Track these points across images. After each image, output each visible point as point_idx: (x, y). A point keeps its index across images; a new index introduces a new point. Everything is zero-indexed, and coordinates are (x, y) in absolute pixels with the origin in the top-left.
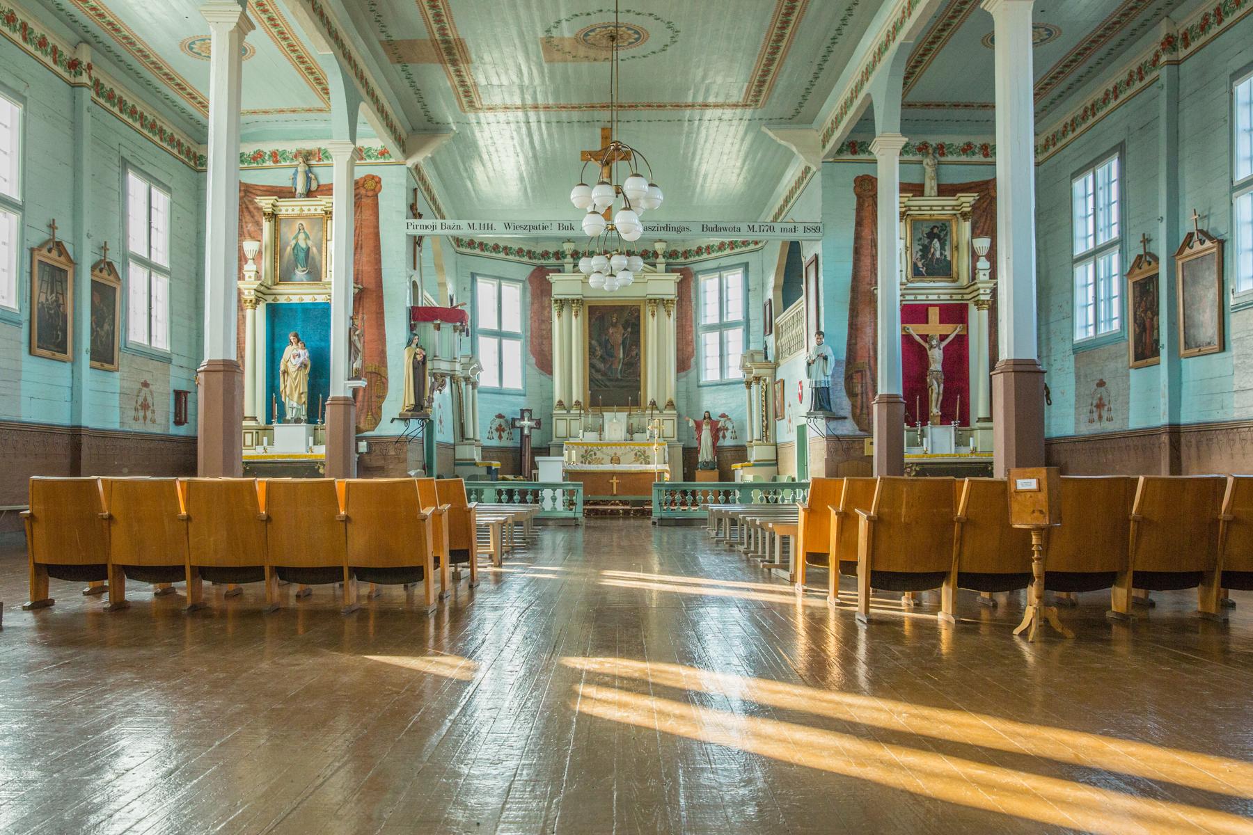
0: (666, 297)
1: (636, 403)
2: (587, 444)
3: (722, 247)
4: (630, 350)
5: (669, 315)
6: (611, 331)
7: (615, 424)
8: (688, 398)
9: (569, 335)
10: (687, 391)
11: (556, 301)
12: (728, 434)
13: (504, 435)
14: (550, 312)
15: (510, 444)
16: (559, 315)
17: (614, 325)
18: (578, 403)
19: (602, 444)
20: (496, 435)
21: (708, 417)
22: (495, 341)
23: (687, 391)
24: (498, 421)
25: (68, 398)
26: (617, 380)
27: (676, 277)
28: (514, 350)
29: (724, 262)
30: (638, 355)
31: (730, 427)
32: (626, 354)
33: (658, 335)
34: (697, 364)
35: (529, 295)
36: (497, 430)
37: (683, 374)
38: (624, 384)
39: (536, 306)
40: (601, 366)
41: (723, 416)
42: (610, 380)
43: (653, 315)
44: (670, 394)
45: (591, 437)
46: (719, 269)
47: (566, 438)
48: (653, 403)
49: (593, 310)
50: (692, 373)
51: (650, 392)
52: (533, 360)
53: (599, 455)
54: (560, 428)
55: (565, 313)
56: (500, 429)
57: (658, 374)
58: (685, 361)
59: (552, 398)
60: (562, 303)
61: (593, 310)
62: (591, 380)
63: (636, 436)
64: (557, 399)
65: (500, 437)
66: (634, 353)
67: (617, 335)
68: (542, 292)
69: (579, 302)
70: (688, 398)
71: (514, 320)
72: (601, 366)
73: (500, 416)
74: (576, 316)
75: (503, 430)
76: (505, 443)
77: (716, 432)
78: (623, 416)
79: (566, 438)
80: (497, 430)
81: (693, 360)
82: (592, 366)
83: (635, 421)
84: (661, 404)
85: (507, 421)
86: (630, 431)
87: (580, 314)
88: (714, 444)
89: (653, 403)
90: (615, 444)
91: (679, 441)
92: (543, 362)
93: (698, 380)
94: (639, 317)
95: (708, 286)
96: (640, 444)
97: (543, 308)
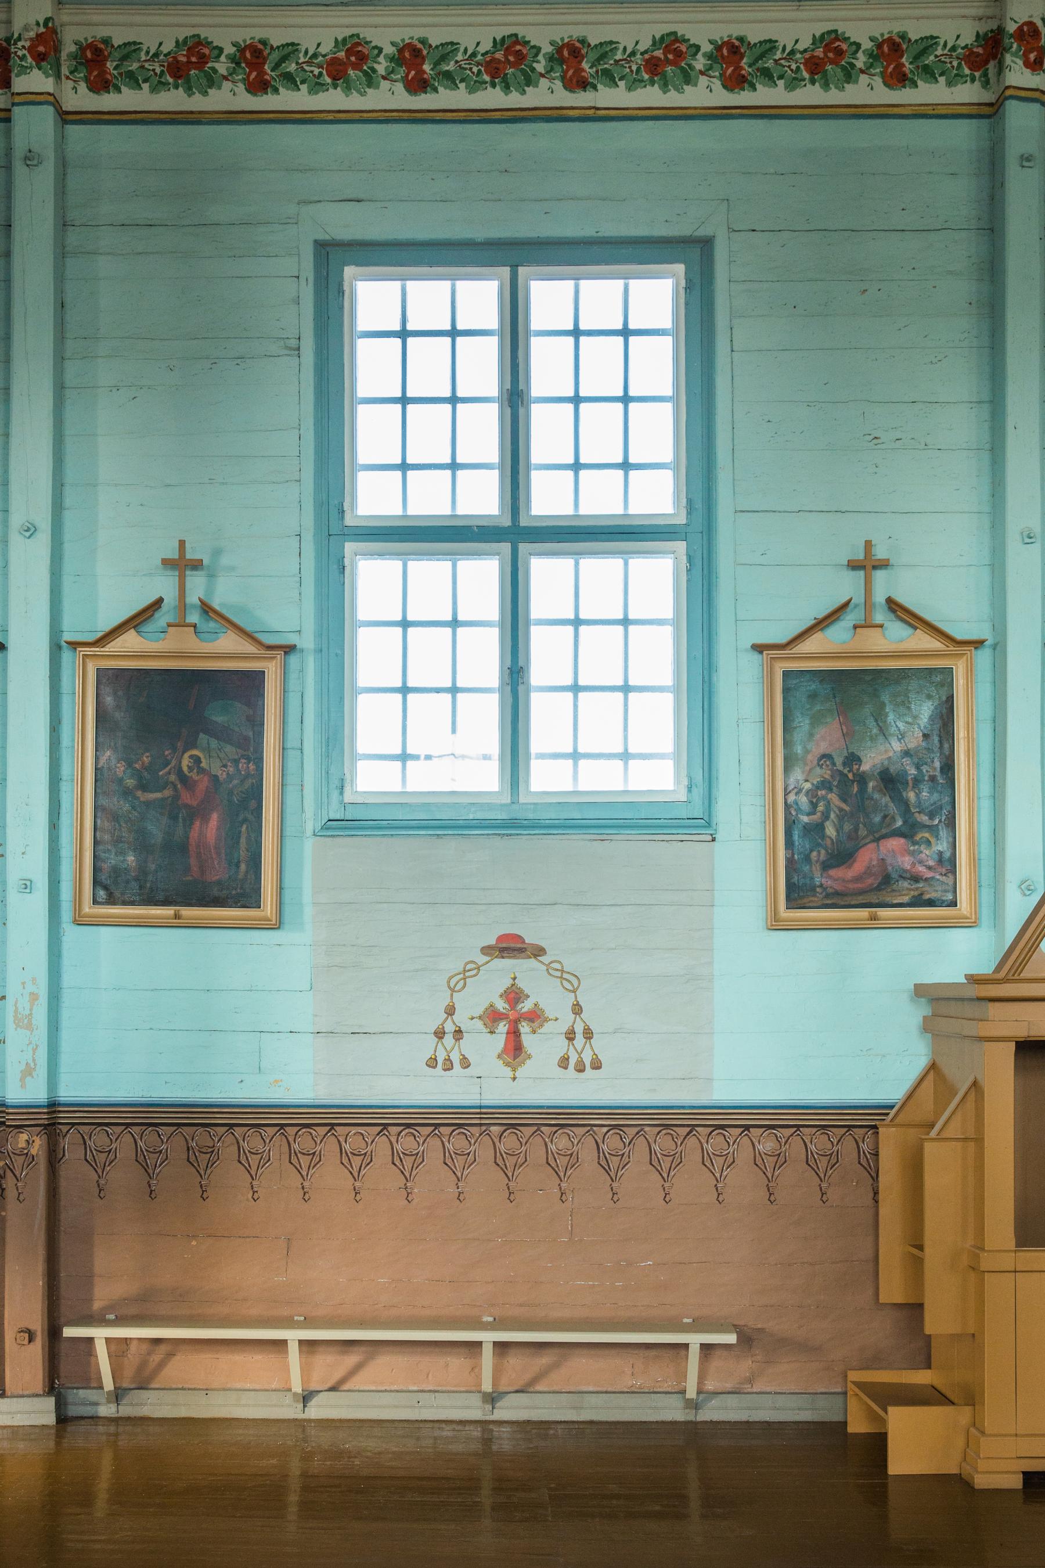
20: (485, 1047)
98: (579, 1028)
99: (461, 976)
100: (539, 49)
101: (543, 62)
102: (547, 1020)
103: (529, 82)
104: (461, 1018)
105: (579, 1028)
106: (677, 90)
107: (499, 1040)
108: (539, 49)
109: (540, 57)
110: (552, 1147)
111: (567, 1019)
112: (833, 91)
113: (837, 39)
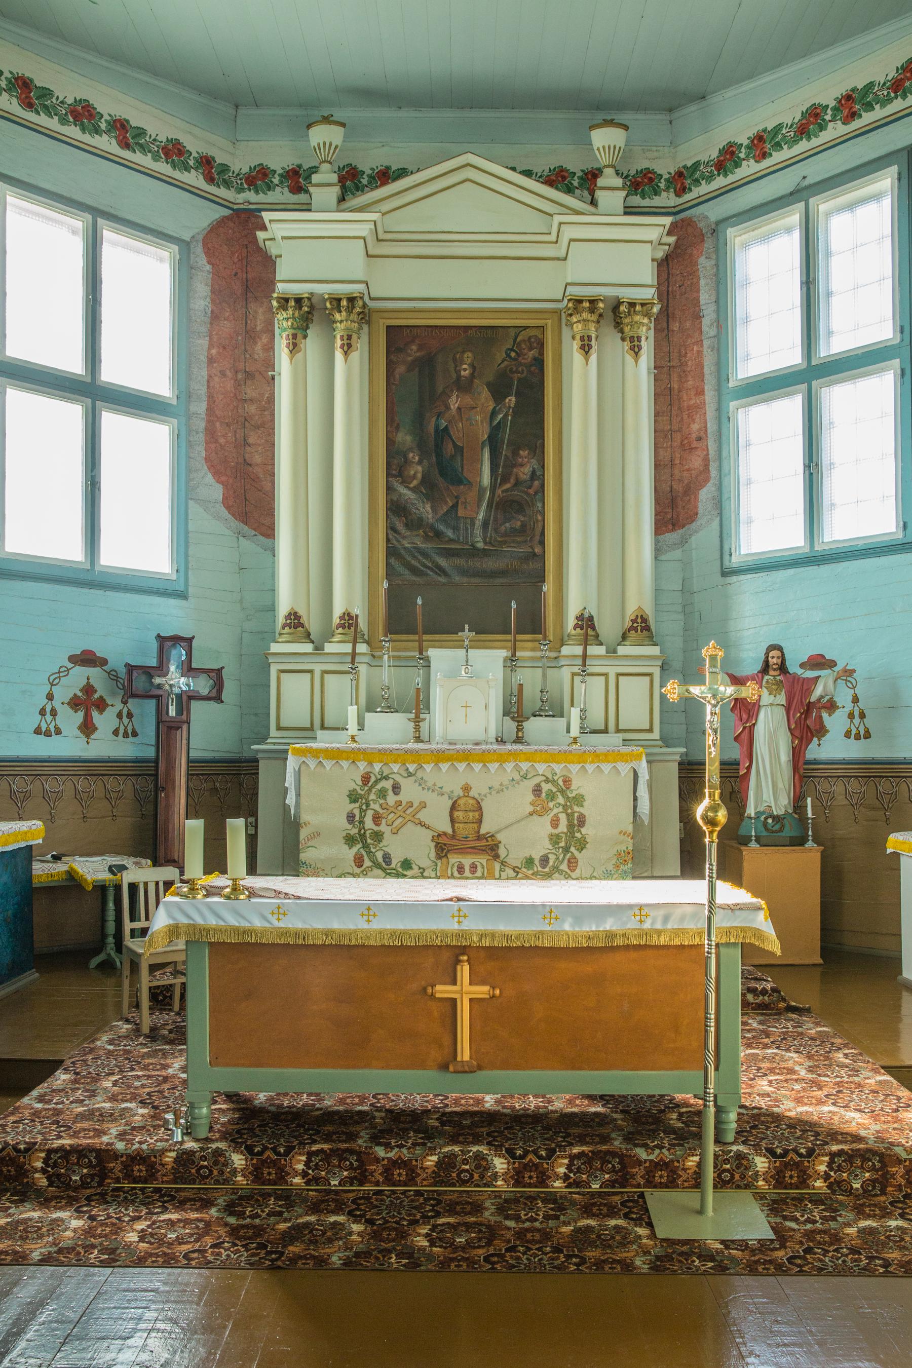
0: (627, 294)
1: (532, 623)
2: (368, 755)
3: (813, 119)
4: (512, 465)
5: (636, 350)
6: (454, 403)
7: (467, 684)
8: (687, 609)
9: (325, 414)
10: (686, 590)
11: (284, 301)
12: (836, 723)
13: (105, 721)
14: (270, 348)
15: (125, 749)
16: (294, 348)
17: (464, 386)
18: (349, 620)
19: (422, 753)
20: (70, 720)
21: (774, 665)
22: (72, 414)
23: (686, 590)
24: (80, 676)
25: (153, 742)
26: (474, 552)
27: (653, 231)
28: (143, 453)
29: (816, 170)
30: (538, 476)
31: (843, 697)
32: (501, 473)
33: (601, 408)
34: (719, 505)
35: (202, 288)
36: (75, 703)
37: (671, 537)
38: (490, 564)
39: (226, 327)
40: (426, 510)
41: (819, 662)
42: (449, 553)
43: (586, 348)
44: (639, 597)
45: (388, 729)
46: (800, 194)
47: (308, 731)
48: (586, 623)
49: (399, 339)
50: (703, 535)
51: (577, 588)
52: (215, 491)
53: (410, 792)
54: (292, 698)
55: (312, 344)
56: (87, 702)
57: (597, 532)
58: (685, 490)
59: (272, 609)
60: (309, 312)
61: (399, 339)
62: (392, 552)
63: (535, 726)
64: (283, 610)
65: (88, 728)
66: (524, 472)
67: (473, 414)
68: (247, 287)
69: (357, 307)
70: (687, 609)
71: (144, 346)
72: (426, 510)
73: (87, 659)
74: (348, 348)
75: (101, 705)
76: (106, 745)
77: (806, 721)
78: (490, 661)
79: (308, 731)
80: (75, 703)
81: (705, 495)
82: (396, 508)
83: (530, 679)
84: (608, 627)
85: (113, 675)
86: (516, 709)
87: (361, 345)
88: (797, 754)
89: (586, 623)
90: (466, 756)
91: (666, 740)
92: (250, 503)
93: (723, 551)
94: (539, 362)
95: (762, 269)
96: (552, 757)
97: (251, 335)
98: (48, 709)
99: (57, 675)
100: (661, 176)
101: (366, 179)
102: (838, 707)
103: (269, 189)
104: (56, 703)
105: (48, 709)
106: (264, 193)
107: (80, 716)
108: (661, 176)
109: (662, 180)
110: (880, 788)
111: (849, 706)
112: (261, 195)
113: (562, 171)
